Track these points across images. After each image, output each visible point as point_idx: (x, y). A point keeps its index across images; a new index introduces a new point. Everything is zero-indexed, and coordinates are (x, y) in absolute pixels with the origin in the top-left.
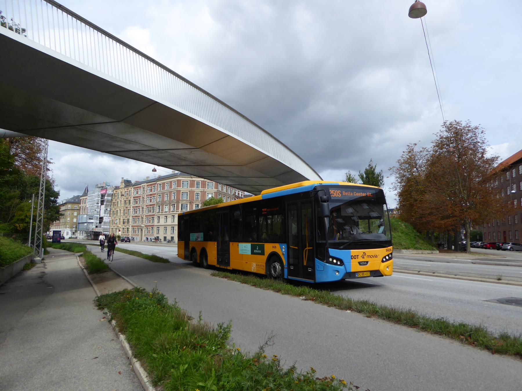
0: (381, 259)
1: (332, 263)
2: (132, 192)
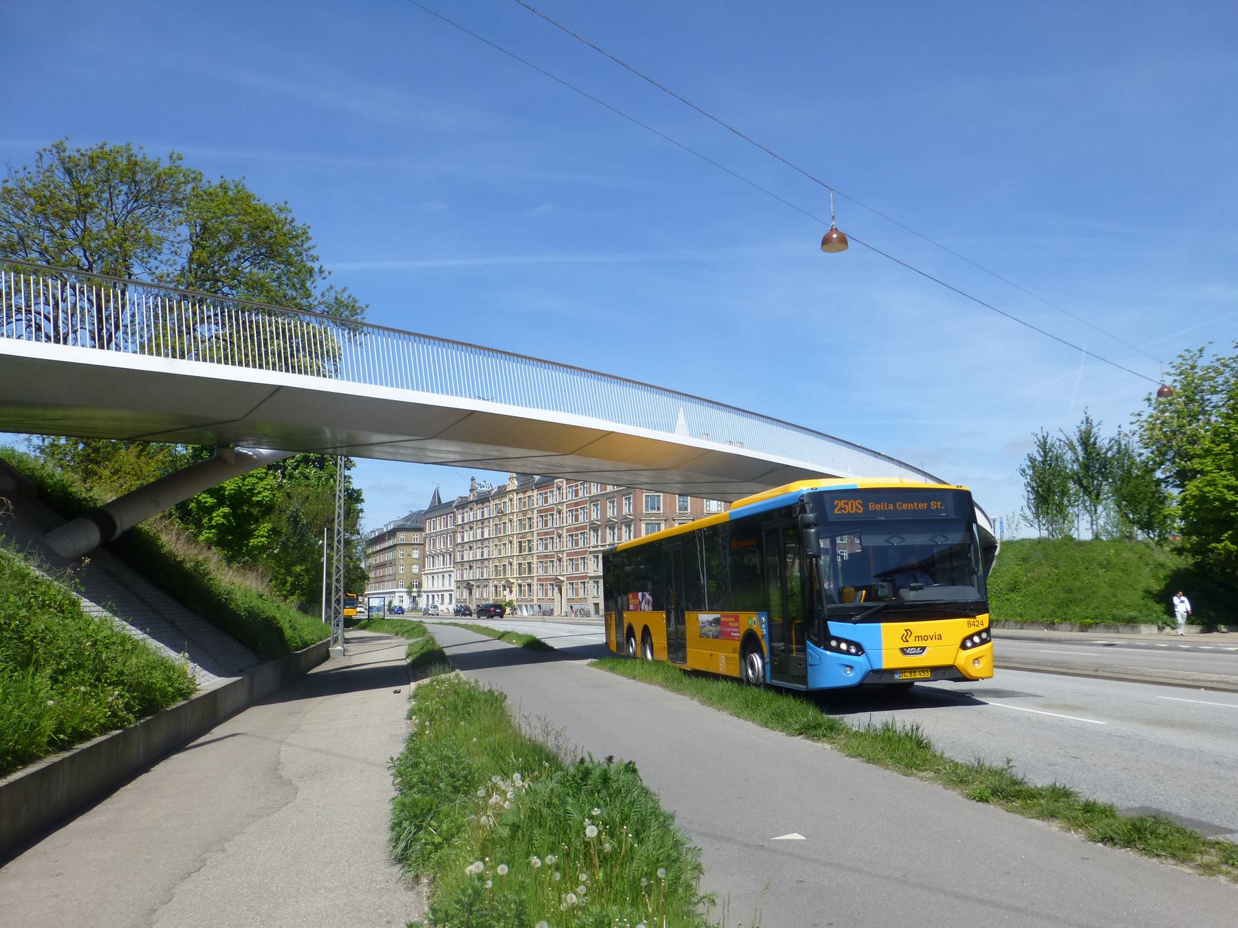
0: (959, 642)
1: (837, 650)
2: (535, 499)
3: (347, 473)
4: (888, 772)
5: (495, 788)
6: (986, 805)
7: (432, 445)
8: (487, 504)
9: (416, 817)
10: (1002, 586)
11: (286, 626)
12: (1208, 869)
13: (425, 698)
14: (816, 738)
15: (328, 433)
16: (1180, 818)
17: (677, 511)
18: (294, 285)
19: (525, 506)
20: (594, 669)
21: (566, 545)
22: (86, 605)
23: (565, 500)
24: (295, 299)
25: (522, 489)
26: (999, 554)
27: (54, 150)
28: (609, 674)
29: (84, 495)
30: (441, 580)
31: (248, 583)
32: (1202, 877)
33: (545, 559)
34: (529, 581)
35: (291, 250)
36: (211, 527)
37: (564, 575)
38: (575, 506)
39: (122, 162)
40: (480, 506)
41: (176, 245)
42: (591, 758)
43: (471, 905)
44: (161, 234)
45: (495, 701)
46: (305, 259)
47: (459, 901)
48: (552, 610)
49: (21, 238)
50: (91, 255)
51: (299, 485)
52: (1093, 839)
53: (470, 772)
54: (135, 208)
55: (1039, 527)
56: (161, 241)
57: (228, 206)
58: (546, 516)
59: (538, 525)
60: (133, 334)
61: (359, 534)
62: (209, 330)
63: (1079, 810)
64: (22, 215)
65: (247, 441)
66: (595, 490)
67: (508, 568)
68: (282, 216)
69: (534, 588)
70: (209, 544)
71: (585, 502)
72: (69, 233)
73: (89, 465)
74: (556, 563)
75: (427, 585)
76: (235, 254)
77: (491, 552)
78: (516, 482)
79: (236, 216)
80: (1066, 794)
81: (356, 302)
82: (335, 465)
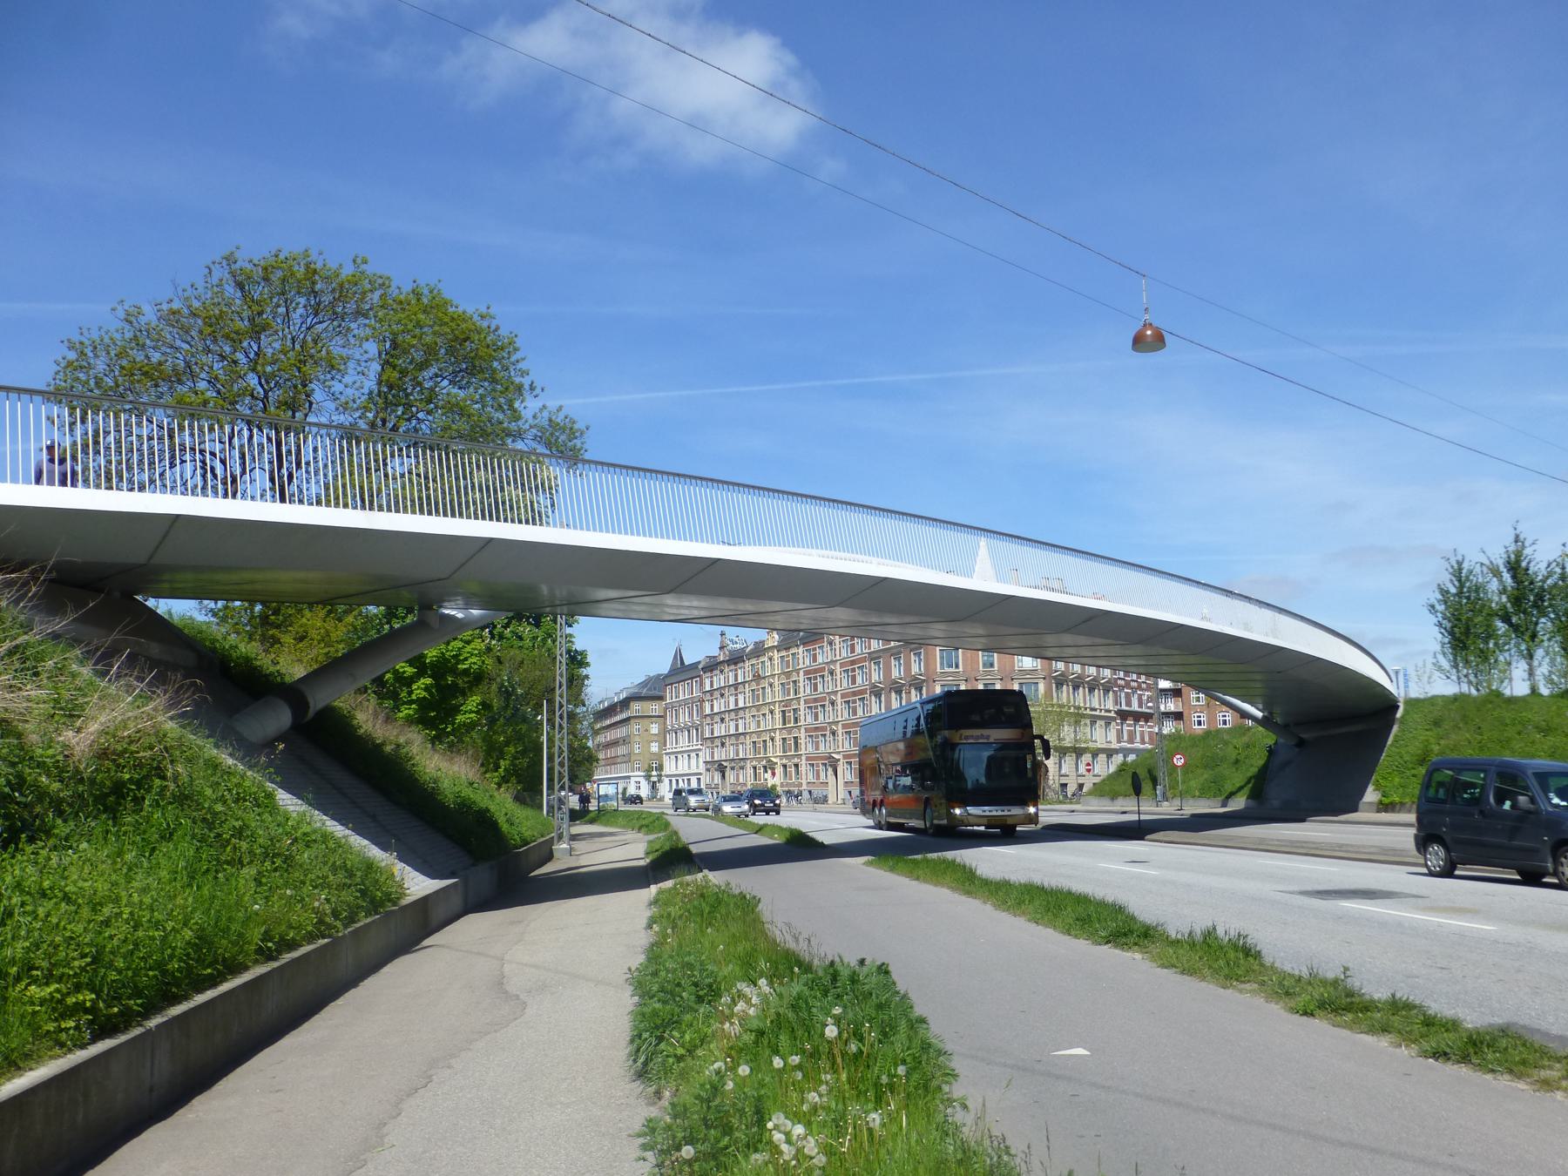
2: (801, 656)
3: (569, 630)
4: (1204, 984)
5: (741, 995)
6: (1311, 1020)
7: (669, 600)
8: (741, 665)
9: (657, 1027)
10: (1407, 758)
11: (502, 820)
12: (1547, 1085)
13: (666, 904)
14: (1124, 946)
15: (545, 590)
16: (1547, 1035)
17: (981, 668)
18: (500, 406)
19: (788, 667)
20: (872, 870)
21: (842, 713)
22: (284, 798)
23: (838, 658)
24: (501, 423)
25: (784, 646)
26: (1403, 717)
27: (224, 263)
28: (888, 874)
29: (272, 669)
30: (686, 761)
31: (456, 768)
32: (1538, 1094)
33: (815, 732)
34: (796, 760)
35: (495, 364)
36: (411, 702)
37: (839, 753)
38: (851, 666)
39: (300, 271)
40: (733, 667)
41: (363, 364)
42: (842, 961)
43: (709, 1101)
44: (344, 352)
45: (747, 905)
46: (512, 374)
47: (698, 1097)
48: (826, 796)
49: (188, 366)
50: (267, 382)
51: (512, 647)
52: (1425, 1054)
53: (715, 981)
54: (316, 323)
55: (1459, 678)
56: (345, 360)
57: (421, 316)
58: (815, 678)
59: (805, 690)
60: (316, 473)
61: (584, 706)
62: (402, 464)
63: (1417, 1024)
64: (189, 339)
65: (449, 601)
66: (875, 645)
67: (769, 744)
68: (485, 324)
69: (803, 769)
70: (410, 721)
71: (864, 660)
72: (240, 356)
73: (268, 627)
74: (830, 738)
75: (669, 767)
76: (433, 370)
77: (748, 724)
78: (777, 637)
79: (431, 326)
80: (1409, 1006)
81: (574, 422)
82: (555, 621)
